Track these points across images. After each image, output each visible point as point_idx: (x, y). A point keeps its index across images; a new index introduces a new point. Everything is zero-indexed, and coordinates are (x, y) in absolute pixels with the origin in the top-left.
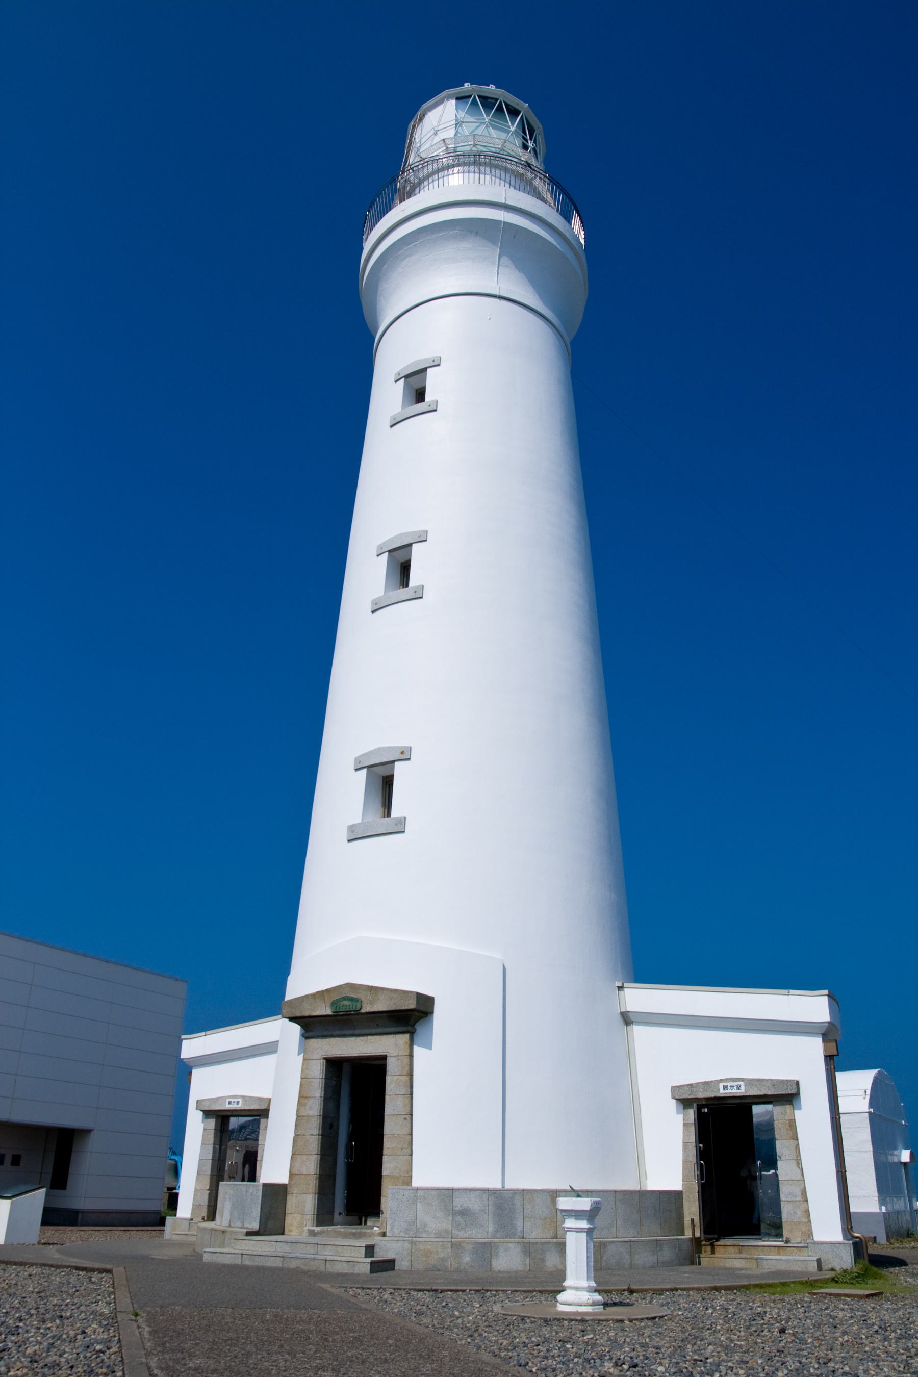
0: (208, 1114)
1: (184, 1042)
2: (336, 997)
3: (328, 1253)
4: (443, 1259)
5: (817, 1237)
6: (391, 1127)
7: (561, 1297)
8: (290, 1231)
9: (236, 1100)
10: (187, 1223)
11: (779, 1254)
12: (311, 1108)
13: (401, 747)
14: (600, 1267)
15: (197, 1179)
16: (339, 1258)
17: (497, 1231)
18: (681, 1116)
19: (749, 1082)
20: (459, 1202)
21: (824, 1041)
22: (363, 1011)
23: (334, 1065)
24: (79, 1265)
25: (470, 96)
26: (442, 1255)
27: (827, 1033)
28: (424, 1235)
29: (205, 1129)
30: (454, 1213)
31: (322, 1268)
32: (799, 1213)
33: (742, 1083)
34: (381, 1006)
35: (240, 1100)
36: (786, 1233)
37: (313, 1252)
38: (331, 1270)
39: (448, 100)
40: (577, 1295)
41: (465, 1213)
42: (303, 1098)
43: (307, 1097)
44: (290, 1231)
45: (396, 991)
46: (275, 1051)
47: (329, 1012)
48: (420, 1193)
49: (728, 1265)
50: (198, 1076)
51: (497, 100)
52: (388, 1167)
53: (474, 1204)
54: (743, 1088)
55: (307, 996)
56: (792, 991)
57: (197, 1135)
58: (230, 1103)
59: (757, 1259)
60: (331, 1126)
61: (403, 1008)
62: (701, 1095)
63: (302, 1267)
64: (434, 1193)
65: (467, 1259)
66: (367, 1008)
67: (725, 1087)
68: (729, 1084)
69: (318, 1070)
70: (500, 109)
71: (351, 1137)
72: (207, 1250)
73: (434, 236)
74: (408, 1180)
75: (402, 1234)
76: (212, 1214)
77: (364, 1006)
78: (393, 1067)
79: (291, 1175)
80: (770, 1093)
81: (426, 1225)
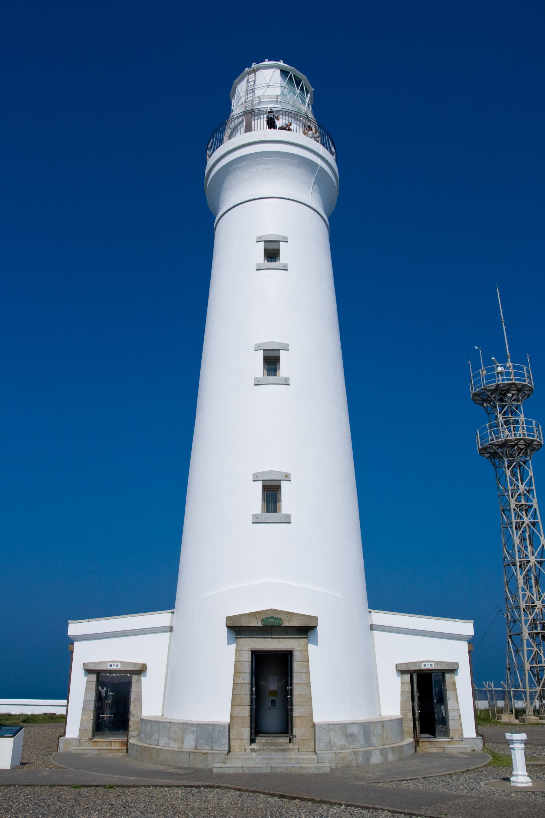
0: (89, 672)
1: (70, 624)
2: (264, 617)
4: (351, 761)
5: (465, 736)
8: (233, 749)
9: (116, 664)
10: (77, 741)
11: (449, 744)
12: (243, 679)
13: (285, 473)
15: (83, 713)
16: (310, 765)
17: (365, 744)
18: (400, 677)
19: (437, 663)
20: (350, 730)
21: (468, 644)
22: (284, 625)
24: (185, 784)
26: (350, 759)
27: (471, 641)
28: (334, 749)
29: (87, 682)
30: (348, 736)
31: (299, 771)
32: (458, 725)
33: (433, 663)
34: (296, 623)
35: (119, 664)
36: (451, 735)
37: (283, 762)
38: (304, 772)
39: (276, 68)
41: (352, 735)
42: (237, 673)
43: (240, 673)
44: (233, 749)
45: (305, 615)
47: (260, 625)
48: (332, 727)
49: (429, 751)
50: (78, 647)
51: (289, 73)
53: (355, 730)
54: (433, 665)
55: (244, 615)
56: (457, 620)
57: (80, 686)
58: (111, 665)
59: (443, 748)
61: (310, 625)
62: (413, 668)
63: (285, 771)
64: (338, 726)
65: (360, 760)
66: (286, 624)
67: (425, 665)
68: (427, 663)
69: (247, 657)
72: (215, 765)
73: (282, 159)
75: (324, 749)
77: (284, 623)
79: (232, 717)
80: (446, 668)
81: (335, 743)
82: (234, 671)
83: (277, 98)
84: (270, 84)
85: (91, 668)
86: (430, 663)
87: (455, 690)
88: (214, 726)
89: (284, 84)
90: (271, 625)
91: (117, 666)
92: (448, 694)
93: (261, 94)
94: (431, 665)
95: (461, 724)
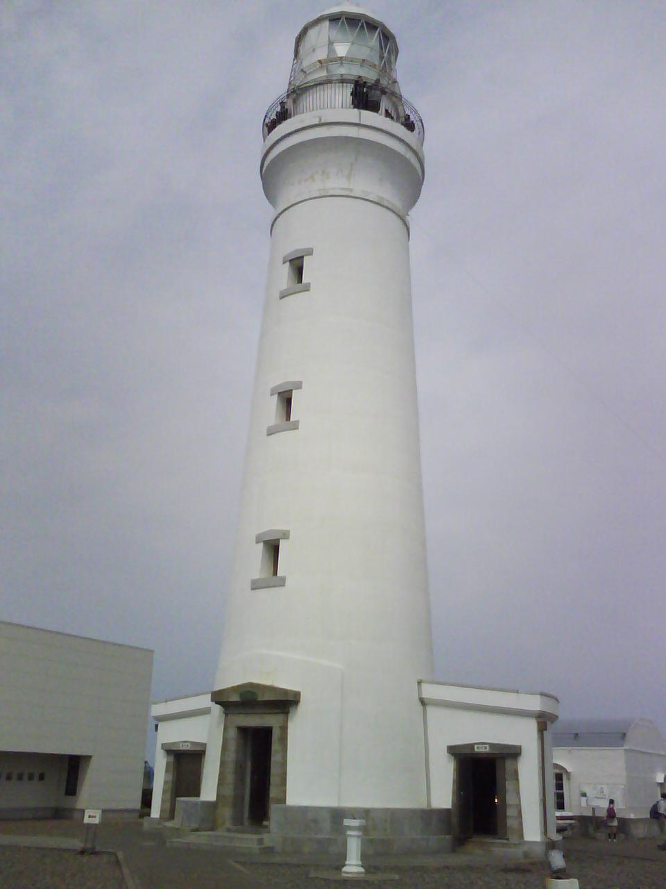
3: (238, 844)
6: (274, 770)
7: (345, 869)
14: (364, 857)
23: (243, 731)
25: (340, 19)
33: (488, 746)
40: (353, 866)
46: (301, 388)
51: (360, 20)
52: (273, 792)
57: (161, 766)
60: (241, 767)
66: (260, 699)
67: (478, 748)
68: (480, 746)
69: (233, 733)
70: (362, 26)
71: (253, 773)
74: (284, 801)
76: (172, 816)
78: (276, 734)
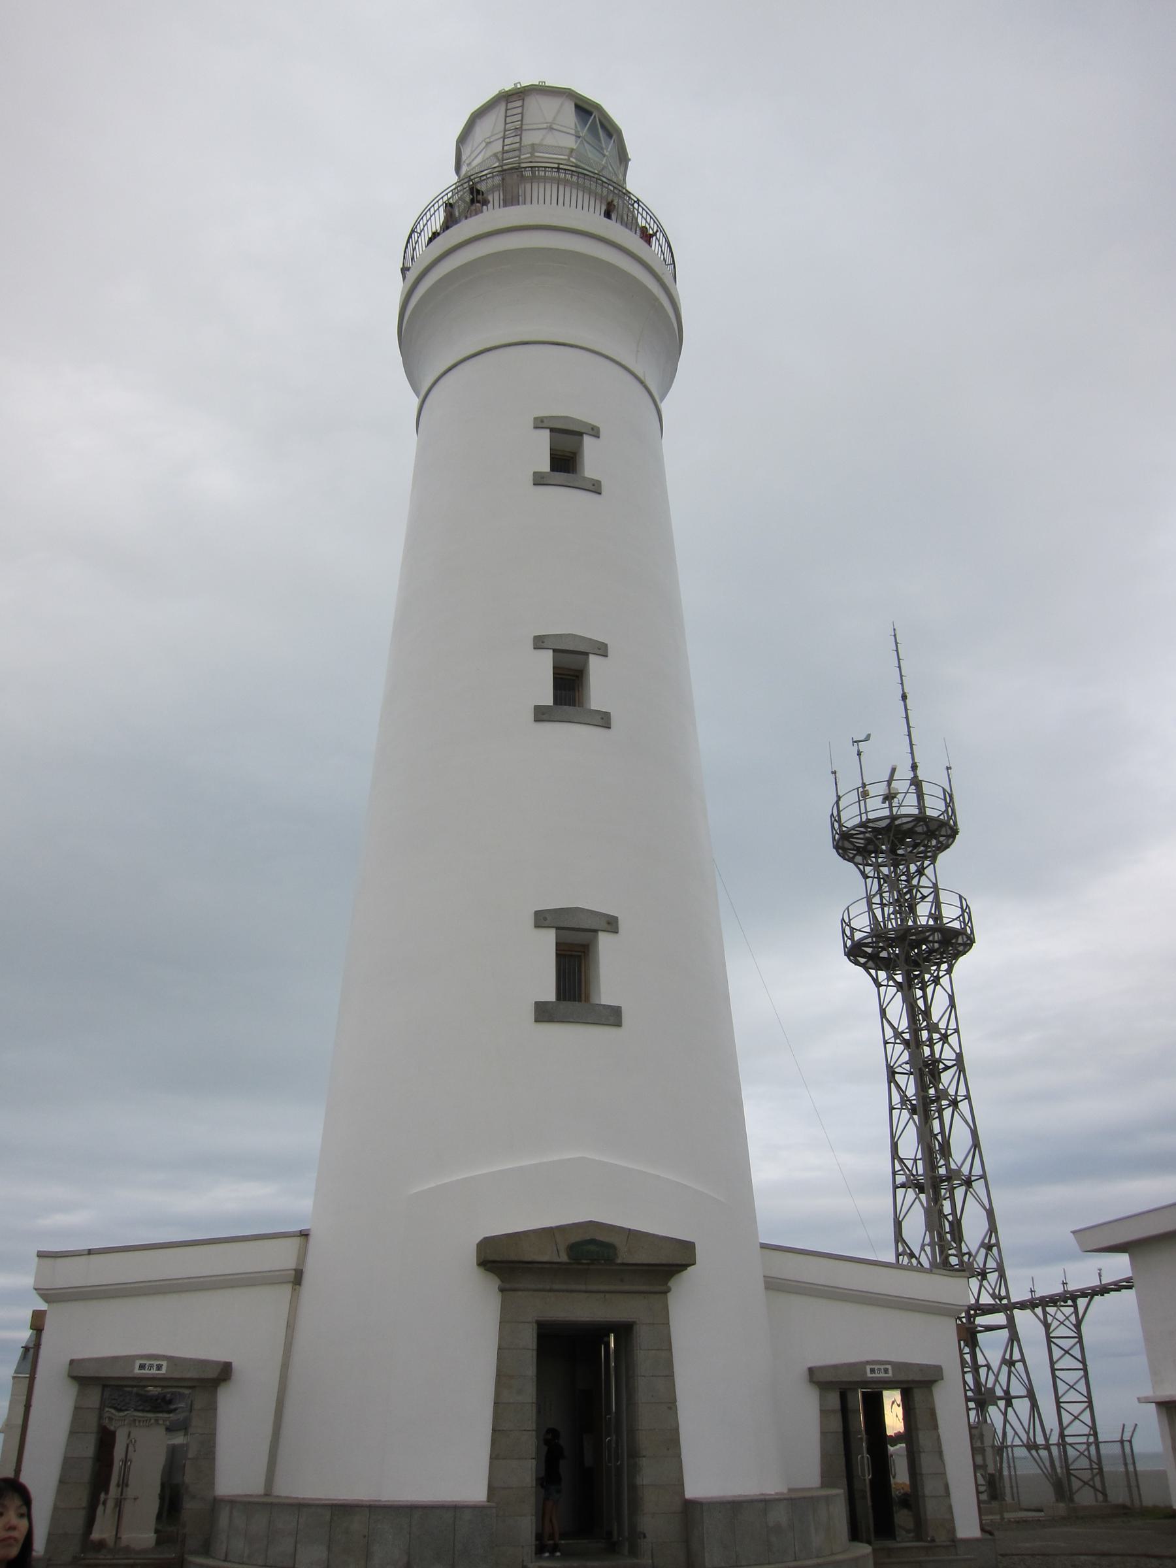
2: (574, 1239)
67: (872, 1371)
68: (876, 1367)
82: (498, 1370)
83: (570, 155)
84: (555, 126)
85: (91, 1372)
86: (882, 1367)
87: (936, 1427)
88: (456, 1509)
89: (584, 132)
90: (590, 1254)
91: (159, 1367)
92: (920, 1436)
93: (537, 141)
94: (886, 1371)
95: (950, 1507)
